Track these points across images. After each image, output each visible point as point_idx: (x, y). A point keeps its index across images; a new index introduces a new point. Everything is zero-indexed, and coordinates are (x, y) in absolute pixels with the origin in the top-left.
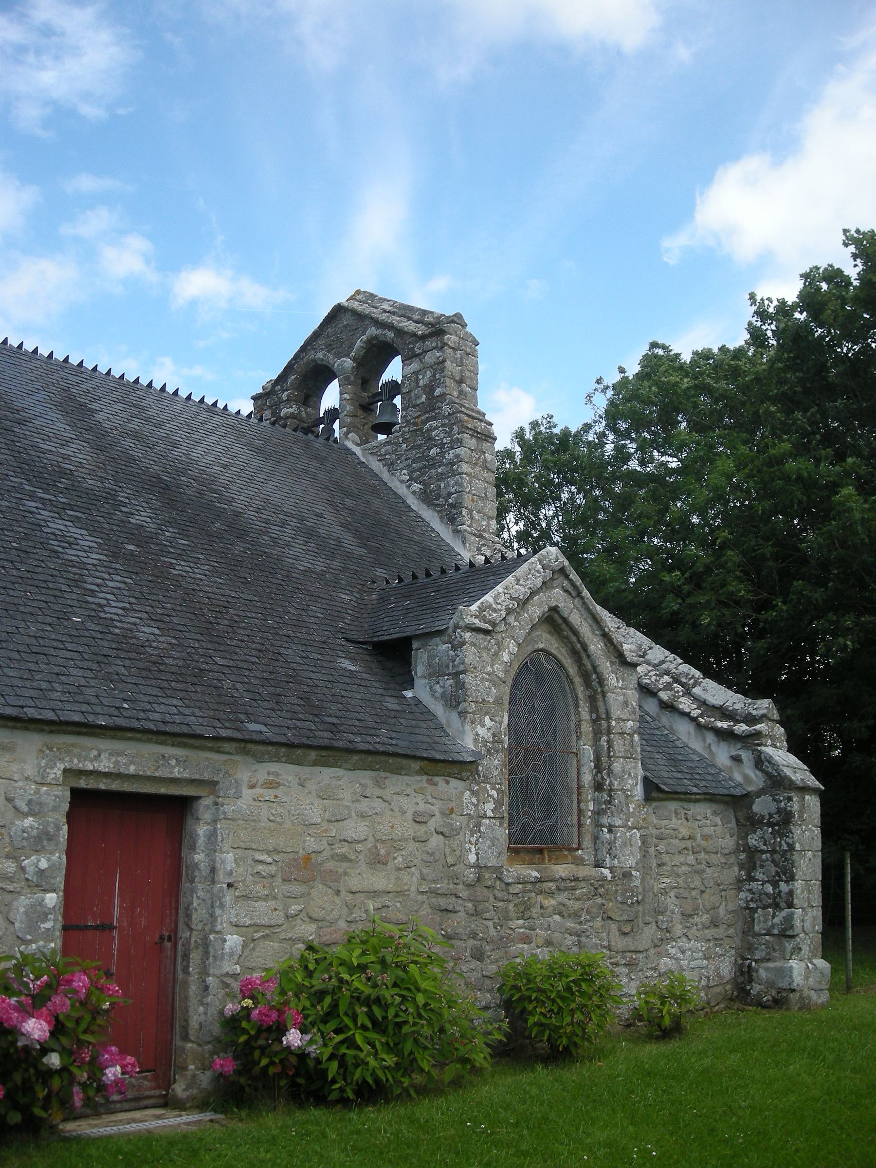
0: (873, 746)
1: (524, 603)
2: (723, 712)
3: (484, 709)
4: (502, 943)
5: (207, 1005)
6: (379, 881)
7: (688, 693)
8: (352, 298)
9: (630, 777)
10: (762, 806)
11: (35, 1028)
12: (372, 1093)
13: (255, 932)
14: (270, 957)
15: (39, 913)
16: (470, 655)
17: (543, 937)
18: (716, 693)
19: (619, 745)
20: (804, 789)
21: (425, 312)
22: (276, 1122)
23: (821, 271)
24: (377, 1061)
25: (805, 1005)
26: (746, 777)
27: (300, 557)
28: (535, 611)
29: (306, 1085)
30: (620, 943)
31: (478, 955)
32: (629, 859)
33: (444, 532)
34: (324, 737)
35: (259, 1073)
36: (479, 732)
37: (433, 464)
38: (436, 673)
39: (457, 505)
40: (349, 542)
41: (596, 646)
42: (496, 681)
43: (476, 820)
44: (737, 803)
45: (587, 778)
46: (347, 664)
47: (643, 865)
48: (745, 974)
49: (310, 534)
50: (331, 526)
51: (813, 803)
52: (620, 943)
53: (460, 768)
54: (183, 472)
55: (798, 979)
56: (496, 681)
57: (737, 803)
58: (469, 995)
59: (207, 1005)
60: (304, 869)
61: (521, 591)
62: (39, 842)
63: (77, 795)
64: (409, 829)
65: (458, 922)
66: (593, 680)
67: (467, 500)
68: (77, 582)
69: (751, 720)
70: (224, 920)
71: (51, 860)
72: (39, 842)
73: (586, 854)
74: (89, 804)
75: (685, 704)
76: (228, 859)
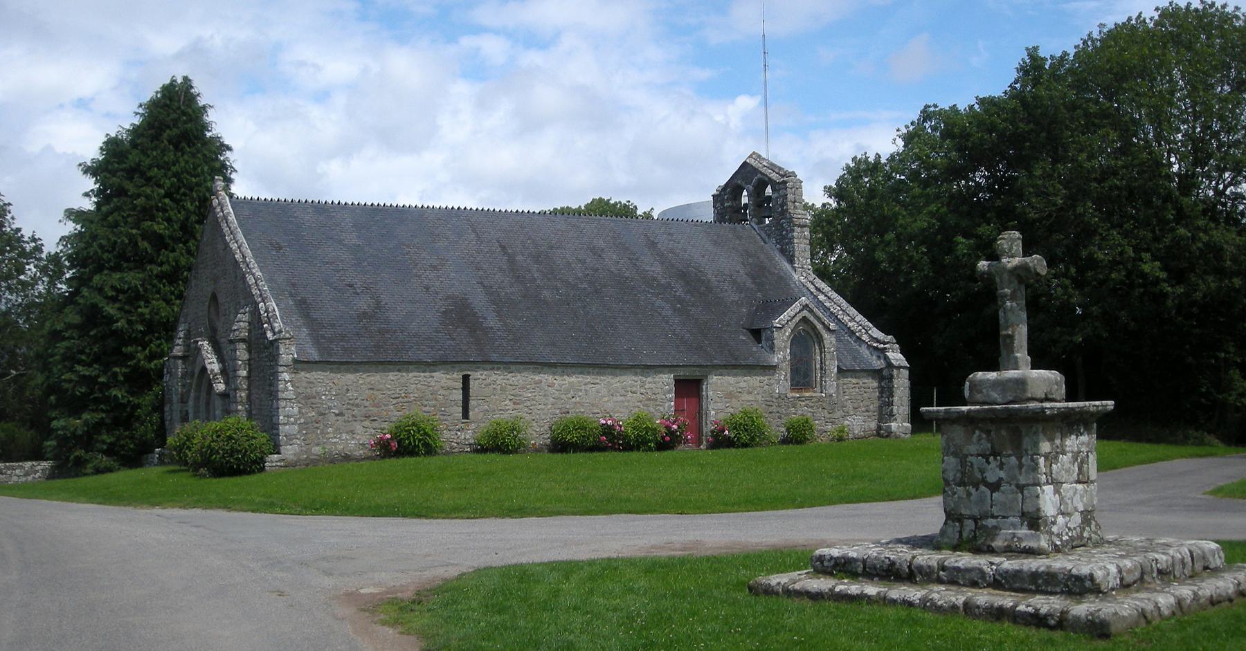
2: (878, 341)
3: (780, 349)
4: (787, 415)
5: (708, 428)
6: (750, 398)
8: (750, 156)
10: (885, 373)
11: (675, 427)
12: (745, 445)
13: (718, 411)
14: (722, 416)
15: (670, 407)
17: (799, 412)
19: (828, 356)
21: (780, 169)
23: (976, 107)
24: (745, 438)
25: (897, 437)
26: (878, 364)
27: (732, 296)
28: (797, 319)
29: (729, 443)
30: (828, 416)
31: (780, 418)
33: (787, 266)
34: (734, 362)
35: (720, 441)
36: (781, 356)
37: (784, 237)
38: (767, 340)
39: (793, 256)
40: (749, 284)
41: (819, 326)
43: (781, 382)
46: (742, 337)
47: (837, 392)
48: (879, 428)
49: (734, 282)
50: (743, 277)
52: (828, 416)
53: (772, 368)
54: (689, 266)
55: (893, 429)
56: (783, 341)
57: (876, 374)
58: (776, 429)
59: (708, 428)
60: (730, 395)
61: (793, 314)
63: (676, 381)
65: (774, 409)
67: (797, 254)
68: (667, 323)
69: (885, 343)
73: (818, 389)
74: (679, 383)
75: (865, 337)
76: (711, 393)
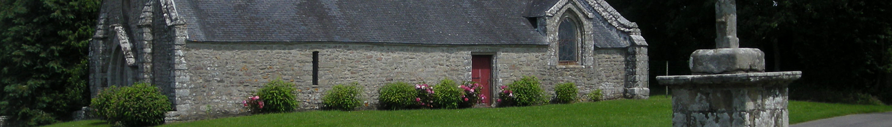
0: (775, 4)
1: (560, 9)
6: (528, 69)
7: (616, 20)
9: (590, 45)
10: (630, 50)
11: (472, 90)
12: (525, 104)
16: (548, 21)
17: (566, 79)
18: (623, 20)
20: (640, 46)
22: (506, 109)
24: (525, 98)
25: (639, 98)
28: (564, 10)
29: (513, 103)
31: (551, 84)
32: (590, 64)
34: (516, 42)
35: (506, 101)
36: (552, 37)
41: (580, 15)
42: (554, 26)
43: (552, 57)
44: (623, 51)
45: (580, 45)
47: (594, 64)
48: (626, 91)
51: (645, 50)
53: (545, 47)
56: (554, 26)
57: (623, 51)
58: (548, 92)
60: (513, 67)
61: (560, 6)
62: (468, 64)
63: (473, 56)
64: (535, 59)
65: (546, 77)
66: (581, 25)
68: (466, 13)
69: (629, 28)
70: (499, 76)
71: (470, 67)
72: (468, 64)
73: (579, 62)
74: (475, 58)
75: (615, 24)
